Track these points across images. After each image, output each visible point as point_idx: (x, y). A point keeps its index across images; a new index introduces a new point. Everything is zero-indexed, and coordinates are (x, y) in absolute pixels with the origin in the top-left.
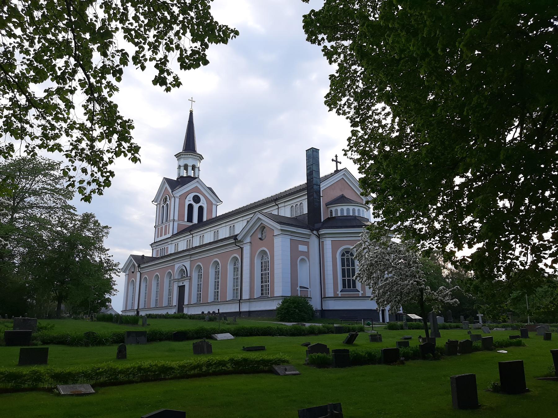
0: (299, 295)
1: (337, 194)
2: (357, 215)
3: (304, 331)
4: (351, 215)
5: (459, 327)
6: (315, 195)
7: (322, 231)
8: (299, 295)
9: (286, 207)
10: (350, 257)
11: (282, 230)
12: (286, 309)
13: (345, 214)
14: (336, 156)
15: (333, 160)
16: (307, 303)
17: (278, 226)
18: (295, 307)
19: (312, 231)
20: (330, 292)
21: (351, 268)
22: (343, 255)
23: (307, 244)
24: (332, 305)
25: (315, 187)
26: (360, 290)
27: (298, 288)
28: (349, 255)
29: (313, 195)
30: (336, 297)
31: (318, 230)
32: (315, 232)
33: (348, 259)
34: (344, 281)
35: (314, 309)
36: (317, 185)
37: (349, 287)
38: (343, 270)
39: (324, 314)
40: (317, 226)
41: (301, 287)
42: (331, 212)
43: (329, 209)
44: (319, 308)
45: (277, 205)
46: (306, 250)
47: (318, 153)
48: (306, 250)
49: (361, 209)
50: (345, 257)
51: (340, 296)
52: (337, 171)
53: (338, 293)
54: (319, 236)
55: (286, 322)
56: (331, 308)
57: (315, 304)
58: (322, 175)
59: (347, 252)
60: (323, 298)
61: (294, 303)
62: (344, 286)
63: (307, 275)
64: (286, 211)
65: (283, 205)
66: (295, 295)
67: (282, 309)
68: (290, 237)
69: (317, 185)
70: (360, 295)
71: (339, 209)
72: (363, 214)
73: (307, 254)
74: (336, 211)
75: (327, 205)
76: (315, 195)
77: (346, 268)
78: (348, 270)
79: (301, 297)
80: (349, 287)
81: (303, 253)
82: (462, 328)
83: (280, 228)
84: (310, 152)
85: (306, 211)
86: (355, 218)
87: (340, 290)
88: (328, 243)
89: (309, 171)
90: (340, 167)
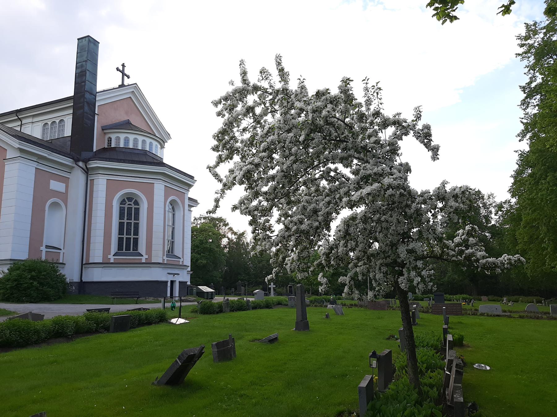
0: (43, 258)
1: (120, 116)
2: (148, 149)
3: (37, 332)
4: (140, 148)
5: (281, 304)
6: (86, 108)
7: (93, 164)
8: (43, 258)
9: (35, 124)
10: (133, 206)
11: (21, 150)
12: (16, 280)
13: (131, 146)
14: (123, 65)
15: (118, 69)
16: (56, 271)
17: (16, 143)
18: (33, 278)
19: (76, 161)
20: (97, 255)
21: (133, 221)
22: (123, 202)
23: (65, 180)
24: (98, 275)
25: (87, 96)
26: (143, 253)
27: (43, 248)
28: (132, 203)
29: (83, 107)
30: (105, 264)
31: (86, 161)
32: (81, 164)
33: (130, 209)
34: (120, 240)
35: (68, 280)
36: (91, 94)
37: (128, 248)
38: (121, 225)
39: (85, 290)
40: (85, 155)
41: (47, 247)
42: (110, 140)
43: (107, 136)
44: (76, 279)
45: (20, 119)
46: (63, 190)
47: (97, 47)
48: (63, 190)
49: (155, 143)
50: (126, 206)
51: (112, 261)
52: (122, 85)
53: (109, 257)
54: (87, 171)
55: (19, 301)
56: (96, 279)
57: (71, 273)
58: (98, 90)
59: (130, 199)
60: (85, 264)
61: (30, 271)
62: (120, 247)
63: (61, 231)
64: (34, 130)
65: (30, 120)
66: (35, 258)
67: (8, 280)
68: (35, 165)
69: (91, 94)
70: (144, 261)
71: (122, 136)
72: (156, 150)
73: (64, 196)
74: (118, 139)
75: (104, 128)
76: (86, 108)
77: (125, 221)
78: (129, 224)
79: (46, 262)
80: (128, 248)
81: (56, 193)
82: (287, 305)
83: (18, 146)
84: (85, 42)
85: (68, 132)
86: (144, 153)
87: (113, 253)
88: (101, 183)
89: (79, 71)
90: (127, 82)
